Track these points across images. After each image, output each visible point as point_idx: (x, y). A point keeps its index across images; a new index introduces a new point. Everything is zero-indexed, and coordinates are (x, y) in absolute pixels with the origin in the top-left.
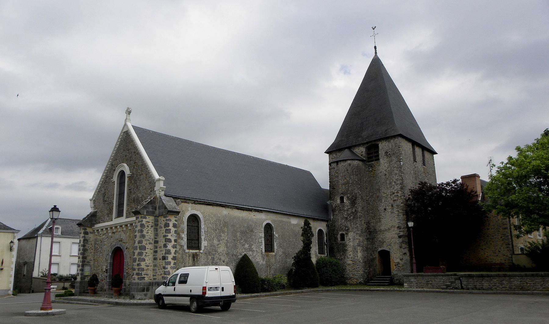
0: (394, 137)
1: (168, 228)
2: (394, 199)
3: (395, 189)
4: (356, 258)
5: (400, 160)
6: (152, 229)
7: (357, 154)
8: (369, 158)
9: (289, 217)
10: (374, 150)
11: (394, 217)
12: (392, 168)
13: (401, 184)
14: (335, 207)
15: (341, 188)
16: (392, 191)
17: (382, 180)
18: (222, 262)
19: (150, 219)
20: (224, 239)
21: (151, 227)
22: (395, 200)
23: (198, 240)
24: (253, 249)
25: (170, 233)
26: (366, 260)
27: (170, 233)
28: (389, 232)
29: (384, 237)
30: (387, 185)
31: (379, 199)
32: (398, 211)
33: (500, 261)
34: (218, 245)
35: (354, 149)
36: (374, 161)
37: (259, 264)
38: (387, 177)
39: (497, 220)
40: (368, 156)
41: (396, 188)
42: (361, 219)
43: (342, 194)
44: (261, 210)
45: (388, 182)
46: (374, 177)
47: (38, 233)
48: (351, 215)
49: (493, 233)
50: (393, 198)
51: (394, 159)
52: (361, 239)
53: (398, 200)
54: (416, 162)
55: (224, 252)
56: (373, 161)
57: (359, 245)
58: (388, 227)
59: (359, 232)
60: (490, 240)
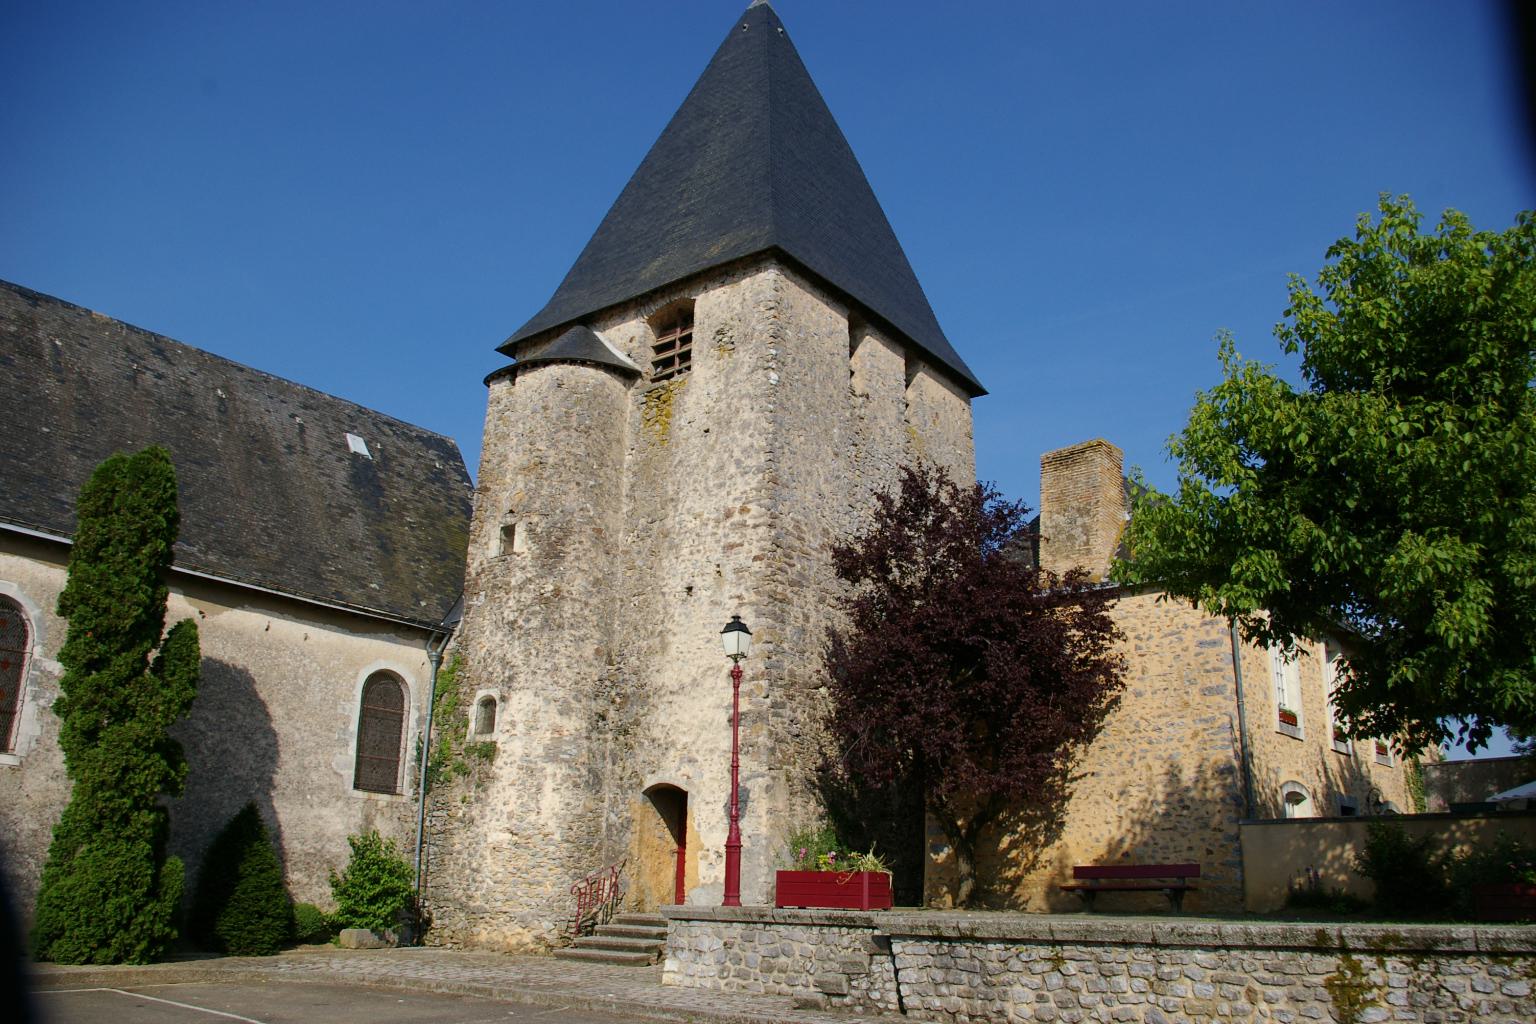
3: (737, 494)
4: (532, 817)
14: (478, 574)
22: (731, 546)
33: (1186, 854)
39: (1178, 651)
41: (741, 488)
47: (961, 860)
48: (533, 613)
49: (1159, 716)
53: (742, 545)
57: (552, 755)
58: (694, 671)
60: (1146, 746)
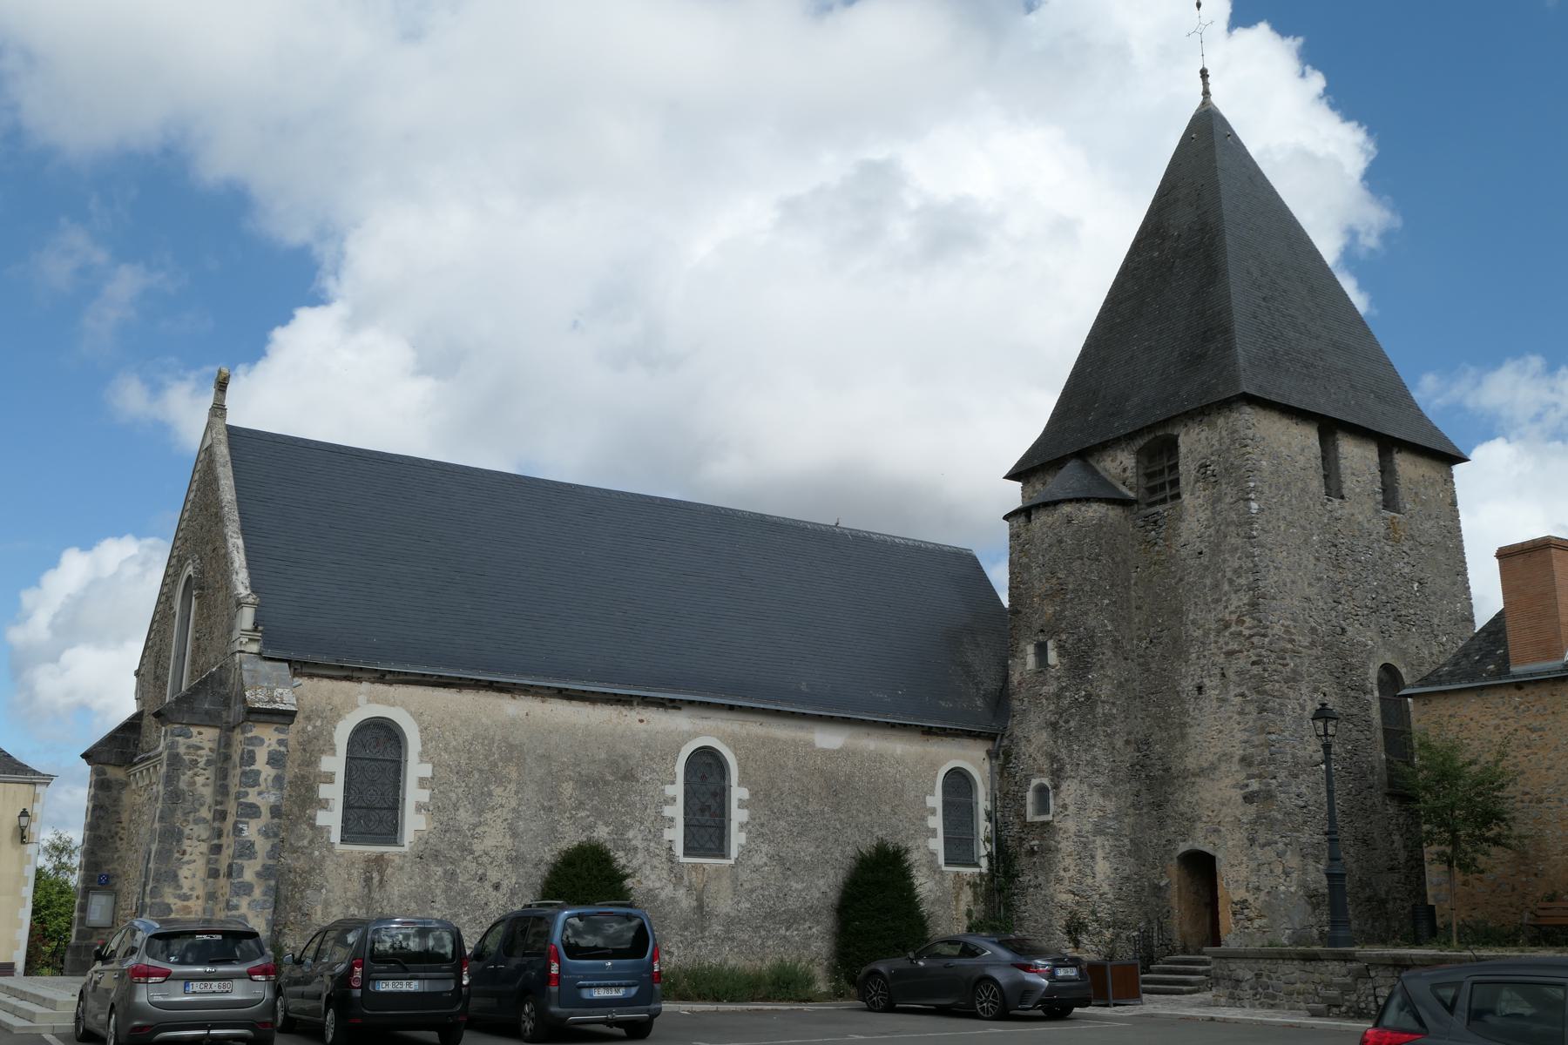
0: (1227, 404)
1: (248, 768)
2: (1230, 647)
3: (1232, 608)
4: (1089, 881)
5: (1246, 497)
6: (210, 773)
7: (1109, 478)
8: (1152, 490)
9: (807, 724)
11: (1230, 718)
12: (1222, 527)
16: (1220, 616)
17: (1190, 573)
18: (491, 889)
19: (206, 737)
20: (502, 806)
21: (205, 764)
23: (394, 806)
24: (630, 840)
25: (256, 784)
27: (256, 784)
28: (1213, 780)
29: (1196, 797)
30: (1205, 594)
31: (1178, 649)
32: (1243, 695)
34: (475, 826)
35: (1098, 461)
36: (1169, 500)
37: (655, 898)
40: (1148, 483)
42: (1110, 726)
43: (1042, 631)
44: (672, 701)
45: (1208, 582)
46: (1161, 563)
48: (1071, 715)
51: (1229, 493)
52: (1111, 806)
53: (1241, 651)
54: (1342, 497)
55: (502, 853)
56: (1163, 501)
57: (1099, 830)
59: (1101, 780)
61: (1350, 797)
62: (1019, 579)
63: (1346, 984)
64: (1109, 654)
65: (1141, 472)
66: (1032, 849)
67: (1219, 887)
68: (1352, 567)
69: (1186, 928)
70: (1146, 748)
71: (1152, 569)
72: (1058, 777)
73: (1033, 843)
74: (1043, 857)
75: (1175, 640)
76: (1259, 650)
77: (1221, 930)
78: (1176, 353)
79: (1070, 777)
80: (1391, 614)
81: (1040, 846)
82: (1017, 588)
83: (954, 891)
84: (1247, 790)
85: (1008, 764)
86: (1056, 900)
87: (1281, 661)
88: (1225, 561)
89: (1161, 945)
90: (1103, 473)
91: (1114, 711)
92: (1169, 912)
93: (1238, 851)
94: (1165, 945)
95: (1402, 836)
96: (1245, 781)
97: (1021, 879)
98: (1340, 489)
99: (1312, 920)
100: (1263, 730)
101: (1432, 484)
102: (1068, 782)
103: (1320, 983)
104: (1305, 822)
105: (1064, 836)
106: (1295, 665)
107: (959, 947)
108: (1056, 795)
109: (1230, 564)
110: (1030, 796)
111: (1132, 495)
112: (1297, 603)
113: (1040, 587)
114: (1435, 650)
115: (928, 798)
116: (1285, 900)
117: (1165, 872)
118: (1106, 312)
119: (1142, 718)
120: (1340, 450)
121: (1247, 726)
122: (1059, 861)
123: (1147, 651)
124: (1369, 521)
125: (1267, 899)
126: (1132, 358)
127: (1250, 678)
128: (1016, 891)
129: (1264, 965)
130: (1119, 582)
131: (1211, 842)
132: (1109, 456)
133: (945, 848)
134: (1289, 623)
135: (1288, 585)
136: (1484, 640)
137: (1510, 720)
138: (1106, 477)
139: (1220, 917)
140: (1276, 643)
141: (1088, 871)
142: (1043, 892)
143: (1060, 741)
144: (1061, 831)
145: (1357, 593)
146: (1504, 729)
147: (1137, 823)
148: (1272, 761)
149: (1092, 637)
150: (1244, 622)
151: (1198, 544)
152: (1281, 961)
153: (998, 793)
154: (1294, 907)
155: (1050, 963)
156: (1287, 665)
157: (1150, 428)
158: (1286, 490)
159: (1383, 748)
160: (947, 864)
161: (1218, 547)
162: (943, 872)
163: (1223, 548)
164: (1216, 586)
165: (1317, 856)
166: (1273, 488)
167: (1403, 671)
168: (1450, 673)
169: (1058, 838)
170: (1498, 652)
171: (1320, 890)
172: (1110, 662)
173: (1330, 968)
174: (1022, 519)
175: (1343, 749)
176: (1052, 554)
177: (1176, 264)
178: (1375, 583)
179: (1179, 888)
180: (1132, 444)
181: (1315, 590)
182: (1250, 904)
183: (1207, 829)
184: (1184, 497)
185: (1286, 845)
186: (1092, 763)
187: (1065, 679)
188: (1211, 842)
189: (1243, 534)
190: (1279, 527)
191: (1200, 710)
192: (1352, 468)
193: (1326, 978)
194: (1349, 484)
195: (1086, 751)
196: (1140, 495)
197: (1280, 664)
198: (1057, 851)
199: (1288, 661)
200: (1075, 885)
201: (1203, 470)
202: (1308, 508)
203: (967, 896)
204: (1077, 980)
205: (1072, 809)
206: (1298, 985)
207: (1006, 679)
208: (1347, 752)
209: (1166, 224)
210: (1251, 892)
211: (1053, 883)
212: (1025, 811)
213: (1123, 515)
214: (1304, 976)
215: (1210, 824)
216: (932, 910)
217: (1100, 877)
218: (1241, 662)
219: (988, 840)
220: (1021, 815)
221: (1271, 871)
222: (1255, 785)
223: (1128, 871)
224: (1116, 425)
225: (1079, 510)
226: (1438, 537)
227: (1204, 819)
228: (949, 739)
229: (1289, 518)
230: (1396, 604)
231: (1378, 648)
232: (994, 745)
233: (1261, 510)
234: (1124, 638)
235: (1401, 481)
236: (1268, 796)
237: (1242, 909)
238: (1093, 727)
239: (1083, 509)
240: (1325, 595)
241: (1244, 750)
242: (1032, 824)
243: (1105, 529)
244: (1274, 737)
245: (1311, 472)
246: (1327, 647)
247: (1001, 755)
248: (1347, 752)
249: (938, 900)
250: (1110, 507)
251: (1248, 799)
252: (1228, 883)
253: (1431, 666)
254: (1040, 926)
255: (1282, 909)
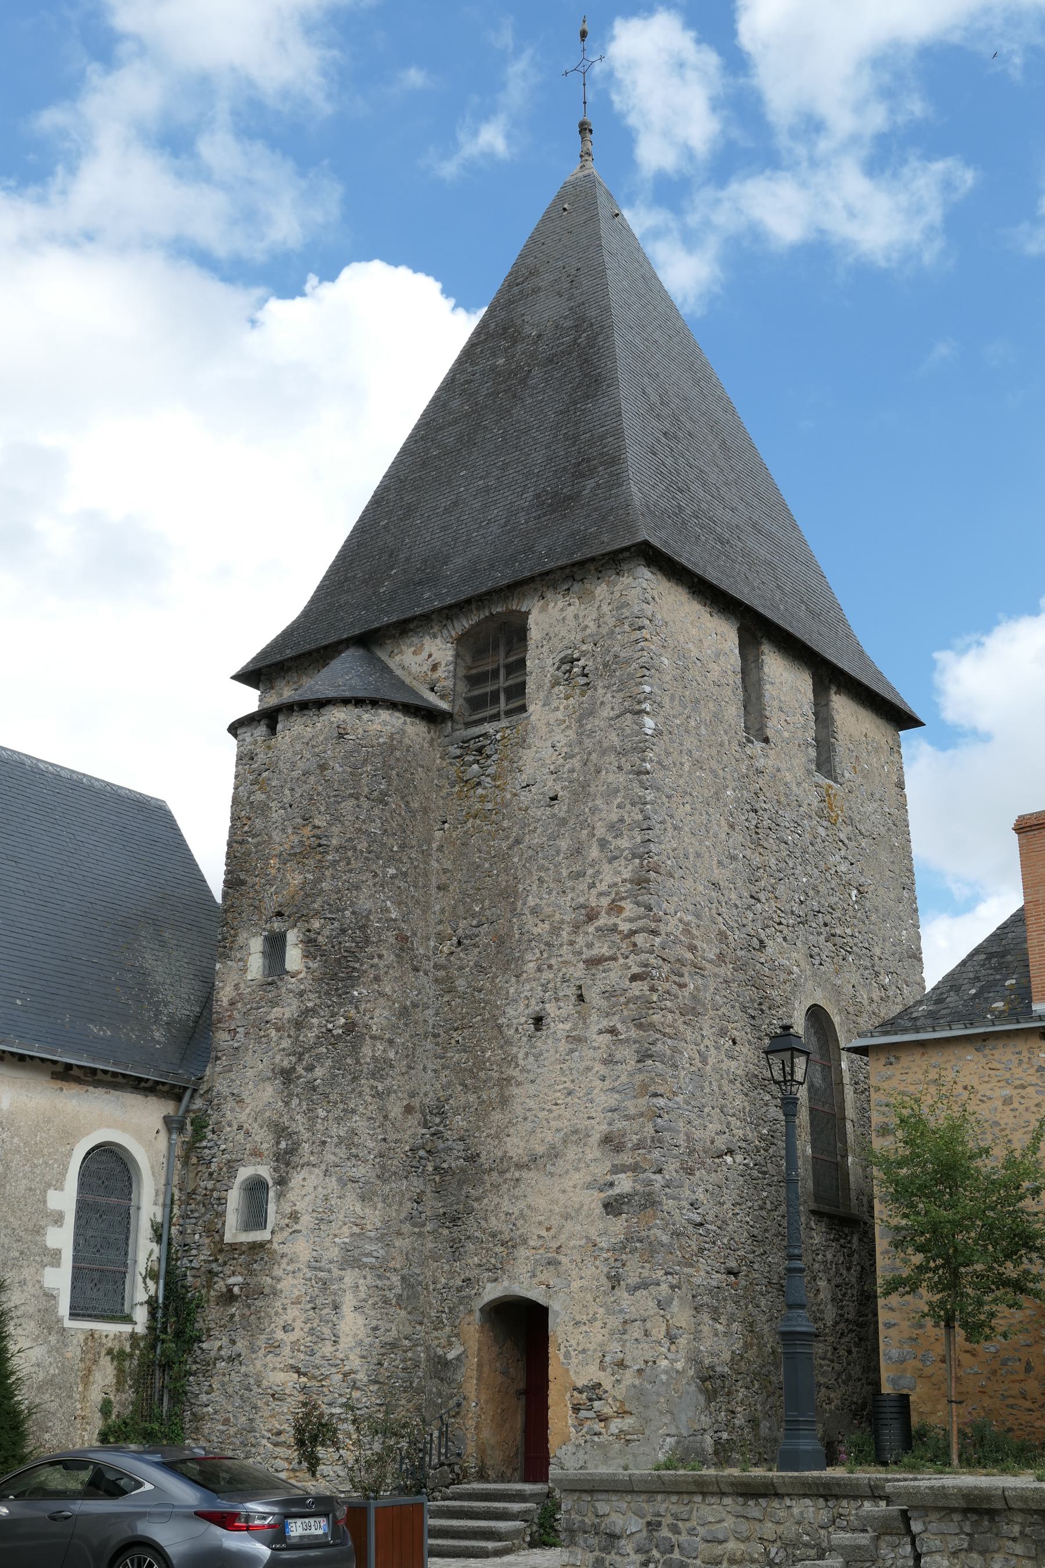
2: (595, 952)
3: (602, 887)
4: (327, 1349)
5: (638, 707)
7: (408, 680)
8: (476, 704)
10: (507, 656)
11: (589, 1069)
12: (594, 756)
13: (634, 856)
15: (275, 878)
16: (582, 900)
17: (534, 831)
26: (394, 1361)
28: (552, 1174)
29: (521, 1204)
32: (612, 1031)
36: (502, 716)
38: (562, 814)
40: (469, 691)
43: (279, 914)
45: (564, 844)
48: (318, 1058)
50: (590, 946)
52: (374, 1217)
53: (614, 958)
54: (766, 740)
56: (496, 717)
57: (351, 1260)
59: (361, 1171)
61: (764, 1213)
62: (246, 828)
63: (859, 1547)
64: (390, 957)
65: (461, 672)
66: (230, 1291)
67: (552, 1362)
68: (775, 848)
69: (486, 1434)
70: (437, 1120)
71: (469, 824)
72: (287, 1164)
73: (232, 1280)
74: (249, 1306)
75: (501, 941)
76: (644, 956)
77: (550, 1438)
78: (529, 495)
79: (308, 1164)
80: (823, 929)
81: (244, 1286)
82: (241, 843)
83: (82, 1365)
84: (610, 1192)
85: (201, 1141)
86: (265, 1383)
87: (677, 979)
88: (594, 810)
89: (442, 1464)
90: (398, 672)
91: (391, 1055)
92: (459, 1405)
93: (589, 1297)
94: (449, 1465)
95: (829, 1280)
96: (609, 1178)
97: (204, 1346)
98: (762, 727)
99: (706, 1420)
100: (644, 1089)
101: (876, 750)
102: (304, 1173)
103: (774, 1542)
104: (701, 1250)
105: (289, 1268)
106: (696, 988)
107: (85, 1475)
108: (280, 1196)
109: (603, 815)
110: (234, 1198)
111: (444, 705)
112: (701, 888)
113: (283, 840)
114: (876, 994)
115: (52, 1195)
116: (666, 1384)
117: (457, 1335)
118: (416, 442)
119: (435, 1071)
120: (766, 669)
121: (616, 1084)
122: (276, 1314)
123: (452, 959)
124: (799, 784)
125: (637, 1382)
126: (455, 504)
127: (627, 1003)
128: (194, 1367)
129: (665, 1505)
130: (414, 843)
131: (541, 1283)
132: (411, 645)
133: (73, 1288)
134: (690, 918)
135: (691, 859)
136: (984, 965)
137: (1030, 1089)
138: (403, 678)
139: (550, 1413)
140: (670, 948)
141: (327, 1331)
142: (243, 1369)
143: (295, 1102)
144: (285, 1261)
145: (781, 888)
146: (1020, 1103)
147: (414, 1249)
148: (657, 1142)
149: (363, 928)
150: (621, 909)
151: (550, 783)
152: (698, 1498)
153: (176, 1192)
154: (680, 1397)
155: (276, 1510)
156: (685, 986)
157: (481, 600)
158: (693, 710)
159: (808, 1138)
160: (74, 1315)
161: (583, 787)
162: (64, 1329)
163: (592, 789)
164: (578, 851)
165: (715, 1310)
166: (676, 702)
167: (836, 1019)
168: (932, 1015)
169: (277, 1272)
170: (1007, 983)
171: (718, 1369)
172: (391, 972)
173: (796, 1511)
174: (262, 730)
175: (756, 1134)
176: (306, 787)
177: (534, 373)
178: (805, 880)
179: (480, 1365)
180: (450, 628)
181: (727, 873)
182: (606, 1392)
183: (536, 1260)
184: (531, 708)
185: (673, 1287)
186: (349, 1141)
187: (312, 996)
188: (541, 1283)
189: (627, 767)
190: (682, 764)
191: (537, 1057)
192: (780, 701)
193: (789, 1530)
194: (774, 725)
195: (338, 1120)
196: (457, 708)
197: (675, 983)
198: (275, 1294)
199: (686, 979)
200: (302, 1356)
201: (567, 667)
202: (721, 745)
203: (105, 1374)
204: (326, 1545)
205: (306, 1221)
206: (732, 1545)
207: (207, 998)
208: (762, 1138)
209: (519, 322)
210: (609, 1370)
211: (262, 1352)
212: (224, 1224)
213: (428, 737)
214: (744, 1527)
215: (541, 1251)
216: (37, 1400)
217: (345, 1342)
218: (614, 975)
219: (152, 1275)
220: (215, 1231)
221: (646, 1333)
222: (625, 1184)
223: (394, 1333)
224: (426, 596)
225: (359, 718)
226: (882, 828)
227: (532, 1243)
228: (99, 1091)
229: (696, 754)
230: (829, 916)
231: (806, 979)
232: (178, 1109)
233: (657, 733)
234: (416, 935)
235: (839, 736)
236: (649, 1202)
237: (591, 1400)
238: (355, 1079)
239: (366, 717)
240: (739, 883)
241: (610, 1124)
242: (234, 1247)
243: (398, 754)
244: (661, 1102)
245: (728, 692)
246: (740, 967)
247: (189, 1128)
248: (762, 1138)
249: (49, 1383)
250: (408, 720)
251: (612, 1207)
252: (567, 1355)
253: (870, 1018)
254: (232, 1431)
255: (662, 1400)
